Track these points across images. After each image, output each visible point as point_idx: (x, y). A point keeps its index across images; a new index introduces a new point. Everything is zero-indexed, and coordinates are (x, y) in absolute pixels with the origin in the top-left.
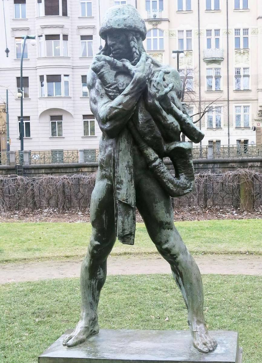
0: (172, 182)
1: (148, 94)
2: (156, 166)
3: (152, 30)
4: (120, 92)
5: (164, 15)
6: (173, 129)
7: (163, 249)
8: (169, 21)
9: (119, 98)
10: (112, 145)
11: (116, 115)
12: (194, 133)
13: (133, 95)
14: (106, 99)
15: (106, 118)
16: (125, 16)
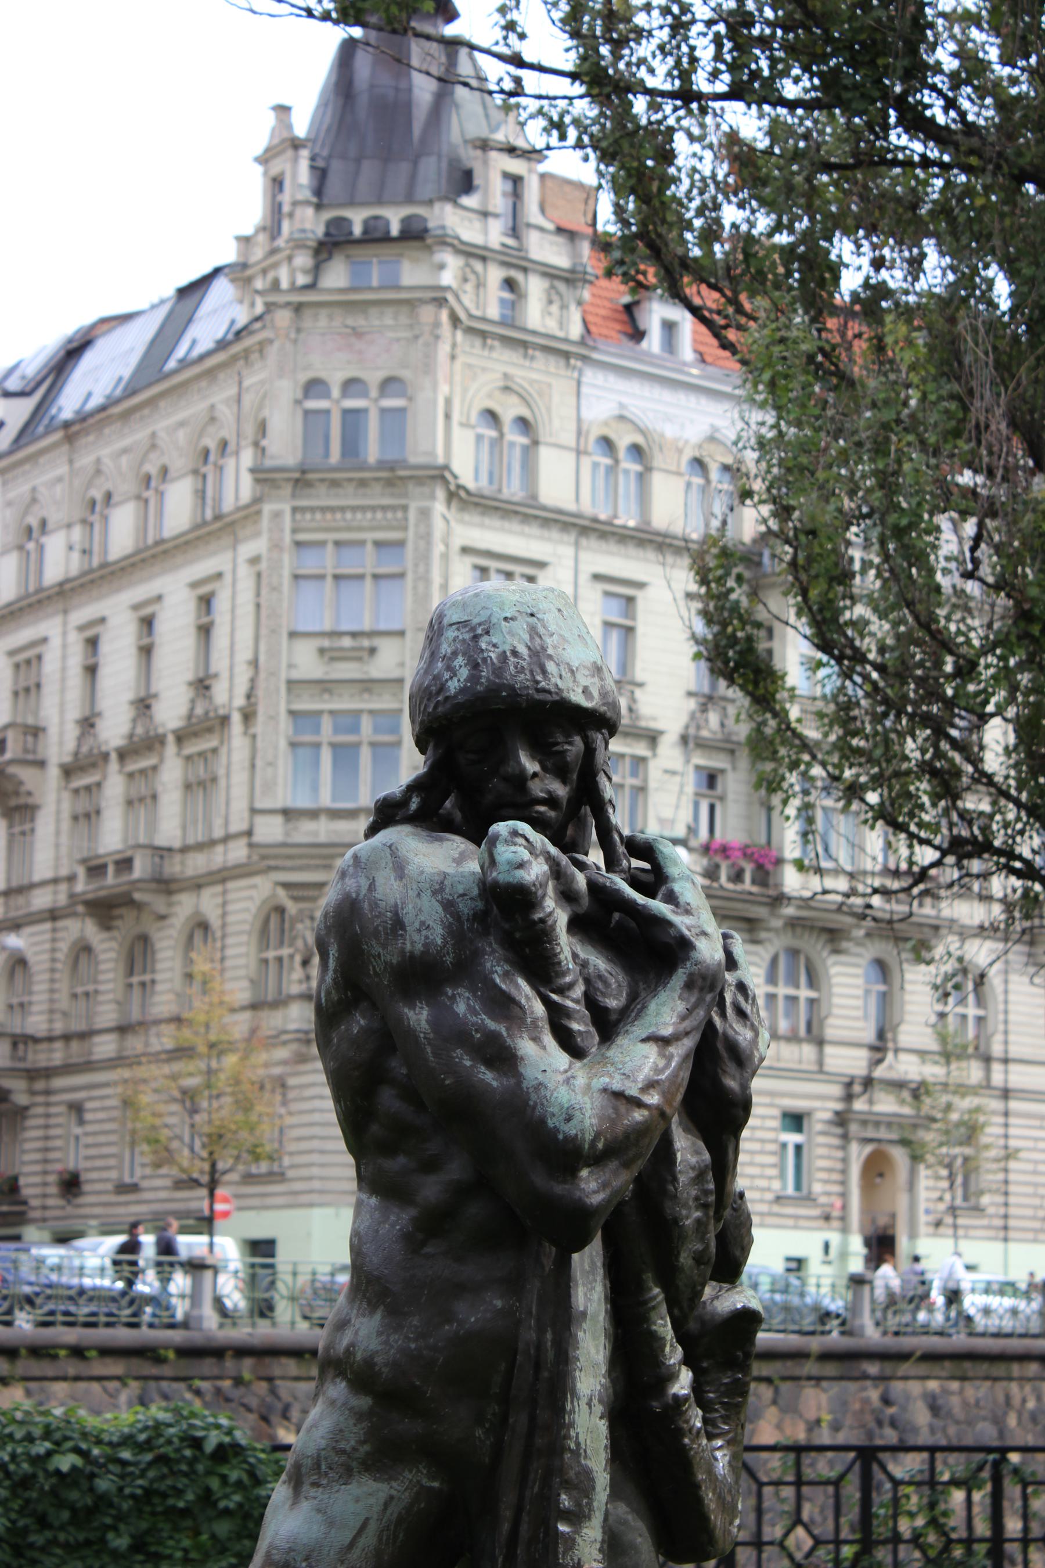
1: (720, 1046)
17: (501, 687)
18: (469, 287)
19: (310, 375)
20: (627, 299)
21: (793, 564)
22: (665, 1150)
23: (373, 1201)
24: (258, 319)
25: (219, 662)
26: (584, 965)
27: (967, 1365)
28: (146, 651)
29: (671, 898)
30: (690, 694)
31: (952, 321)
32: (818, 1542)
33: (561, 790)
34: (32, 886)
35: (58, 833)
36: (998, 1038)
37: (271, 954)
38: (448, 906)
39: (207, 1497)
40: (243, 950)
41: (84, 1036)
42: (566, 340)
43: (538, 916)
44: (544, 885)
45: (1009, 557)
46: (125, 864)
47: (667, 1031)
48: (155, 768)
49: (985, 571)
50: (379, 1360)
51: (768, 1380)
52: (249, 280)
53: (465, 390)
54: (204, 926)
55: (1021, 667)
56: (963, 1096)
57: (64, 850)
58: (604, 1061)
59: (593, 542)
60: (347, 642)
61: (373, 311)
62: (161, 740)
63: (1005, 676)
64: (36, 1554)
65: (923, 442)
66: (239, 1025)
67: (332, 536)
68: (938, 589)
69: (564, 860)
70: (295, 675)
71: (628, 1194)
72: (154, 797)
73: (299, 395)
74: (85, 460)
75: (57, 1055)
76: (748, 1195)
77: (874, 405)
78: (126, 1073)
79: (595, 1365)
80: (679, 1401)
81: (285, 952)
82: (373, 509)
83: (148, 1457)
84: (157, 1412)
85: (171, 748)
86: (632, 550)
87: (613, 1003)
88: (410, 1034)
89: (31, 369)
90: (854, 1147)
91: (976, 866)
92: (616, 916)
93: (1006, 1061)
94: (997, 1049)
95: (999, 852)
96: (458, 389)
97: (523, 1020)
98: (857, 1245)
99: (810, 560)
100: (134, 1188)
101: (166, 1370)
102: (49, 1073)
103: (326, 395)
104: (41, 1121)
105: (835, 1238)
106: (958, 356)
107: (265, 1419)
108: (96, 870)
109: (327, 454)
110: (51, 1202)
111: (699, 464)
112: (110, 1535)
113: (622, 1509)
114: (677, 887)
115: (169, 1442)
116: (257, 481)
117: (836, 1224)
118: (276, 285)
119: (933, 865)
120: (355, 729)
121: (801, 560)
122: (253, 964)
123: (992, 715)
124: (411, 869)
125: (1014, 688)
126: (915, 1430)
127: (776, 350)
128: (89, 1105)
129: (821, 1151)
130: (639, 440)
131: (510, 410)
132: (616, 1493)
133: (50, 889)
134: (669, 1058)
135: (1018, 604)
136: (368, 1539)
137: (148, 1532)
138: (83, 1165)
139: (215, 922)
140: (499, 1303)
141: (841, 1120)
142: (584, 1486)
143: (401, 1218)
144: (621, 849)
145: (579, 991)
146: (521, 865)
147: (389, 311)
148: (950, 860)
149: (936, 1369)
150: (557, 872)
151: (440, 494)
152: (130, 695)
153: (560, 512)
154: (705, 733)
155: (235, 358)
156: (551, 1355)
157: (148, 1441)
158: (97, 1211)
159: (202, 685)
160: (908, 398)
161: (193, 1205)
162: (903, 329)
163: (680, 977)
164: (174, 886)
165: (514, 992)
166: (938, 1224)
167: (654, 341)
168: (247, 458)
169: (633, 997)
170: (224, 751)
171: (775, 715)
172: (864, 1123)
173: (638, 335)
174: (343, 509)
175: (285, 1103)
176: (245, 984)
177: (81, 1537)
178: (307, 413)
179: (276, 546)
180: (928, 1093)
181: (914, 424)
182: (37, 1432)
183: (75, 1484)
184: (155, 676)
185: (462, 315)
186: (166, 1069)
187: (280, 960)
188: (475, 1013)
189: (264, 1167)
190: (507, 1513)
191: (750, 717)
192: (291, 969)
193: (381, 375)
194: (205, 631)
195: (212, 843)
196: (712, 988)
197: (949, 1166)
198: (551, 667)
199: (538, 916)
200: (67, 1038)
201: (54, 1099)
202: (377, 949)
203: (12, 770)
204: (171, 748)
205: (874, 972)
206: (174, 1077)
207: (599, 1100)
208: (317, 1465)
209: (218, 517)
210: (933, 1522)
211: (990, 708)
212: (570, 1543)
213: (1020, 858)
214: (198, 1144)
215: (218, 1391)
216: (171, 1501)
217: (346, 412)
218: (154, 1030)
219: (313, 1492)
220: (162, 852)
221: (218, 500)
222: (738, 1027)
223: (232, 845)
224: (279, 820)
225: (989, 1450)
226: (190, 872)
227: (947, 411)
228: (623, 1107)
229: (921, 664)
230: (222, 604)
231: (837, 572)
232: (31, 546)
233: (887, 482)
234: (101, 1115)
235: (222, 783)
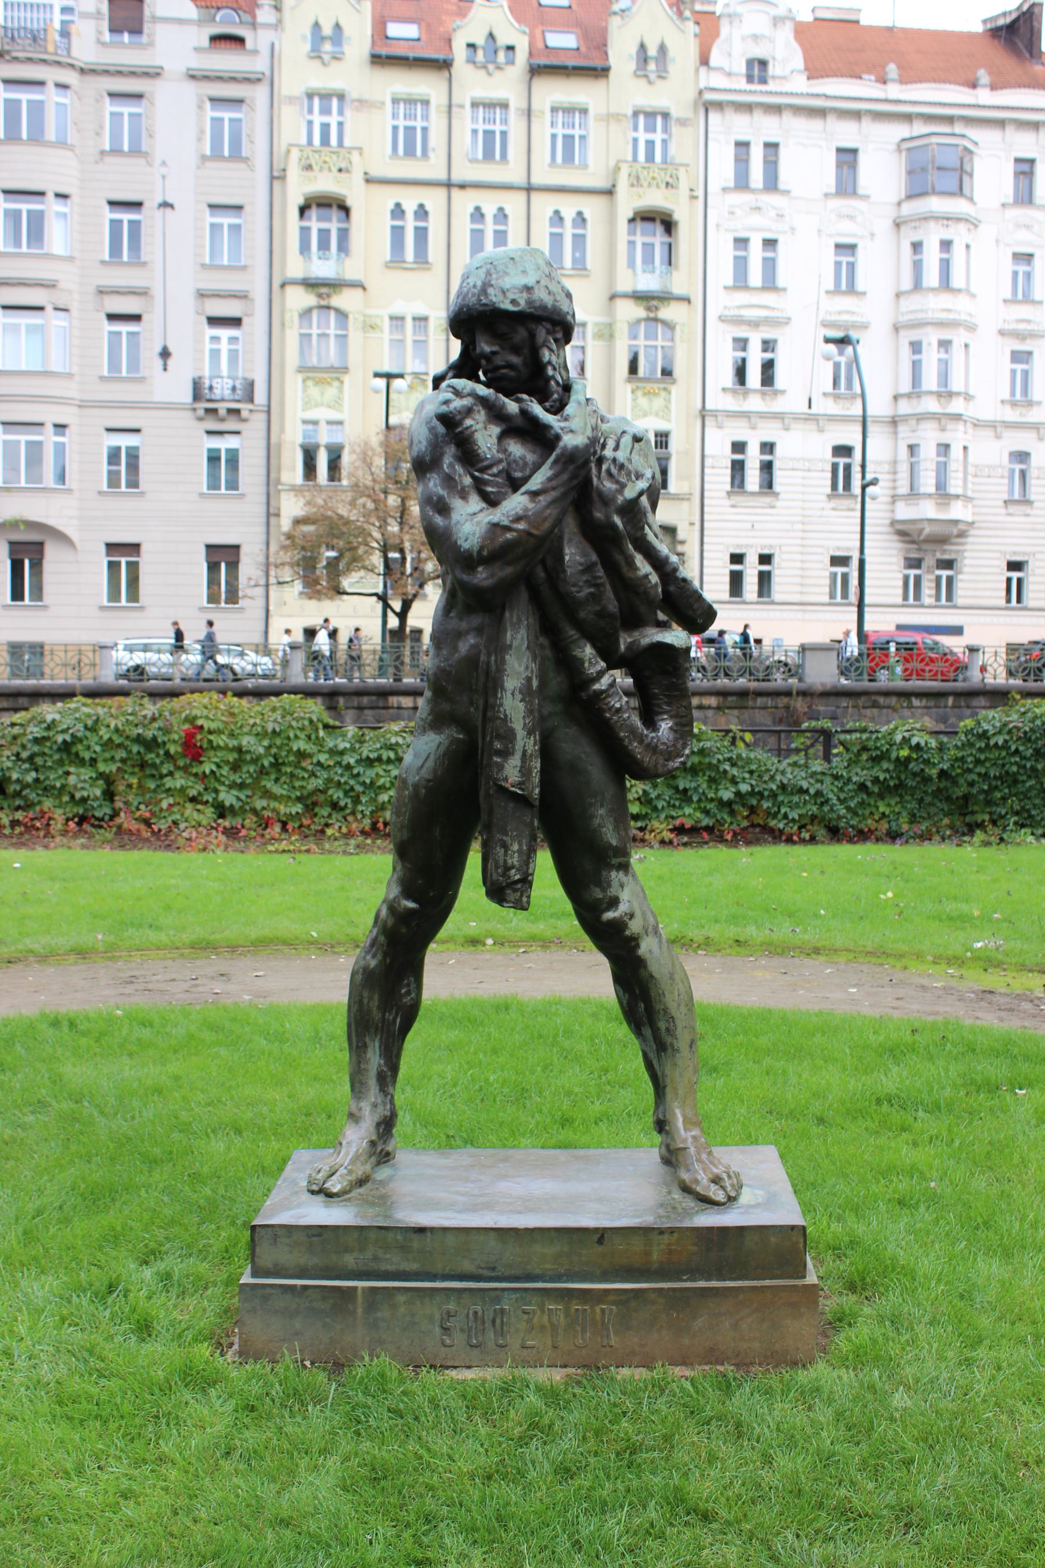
0: (641, 739)
1: (595, 495)
2: (602, 692)
3: (643, 325)
4: (515, 485)
5: (352, 270)
6: (646, 593)
7: (602, 923)
8: (364, 289)
9: (516, 503)
10: (479, 631)
11: (509, 546)
12: (696, 606)
13: (554, 494)
14: (475, 504)
15: (479, 552)
16: (530, 281)
136: (430, 763)
142: (509, 736)
212: (501, 767)
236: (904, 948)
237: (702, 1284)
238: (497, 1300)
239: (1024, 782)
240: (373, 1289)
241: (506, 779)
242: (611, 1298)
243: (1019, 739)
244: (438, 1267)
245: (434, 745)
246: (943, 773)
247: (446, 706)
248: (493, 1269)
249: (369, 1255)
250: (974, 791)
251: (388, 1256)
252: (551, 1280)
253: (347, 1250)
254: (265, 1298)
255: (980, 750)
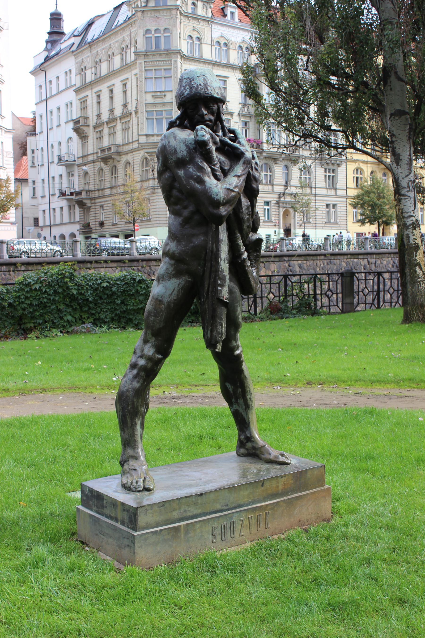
1: (252, 177)
17: (198, 93)
18: (184, 5)
19: (147, 28)
20: (223, 6)
21: (264, 68)
22: (240, 200)
23: (173, 216)
24: (133, 15)
25: (129, 100)
26: (219, 159)
27: (308, 257)
28: (111, 98)
29: (239, 143)
30: (240, 103)
31: (301, 7)
32: (275, 296)
33: (212, 118)
34: (88, 155)
35: (93, 142)
36: (314, 182)
37: (145, 169)
38: (187, 146)
39: (137, 291)
40: (138, 168)
41: (103, 190)
42: (208, 18)
43: (208, 148)
44: (209, 140)
45: (315, 65)
46: (109, 149)
47: (239, 174)
48: (115, 126)
49: (310, 69)
50: (176, 252)
51: (263, 262)
52: (131, 5)
53: (184, 31)
54: (129, 163)
55: (318, 92)
56: (306, 196)
57: (95, 146)
58: (225, 181)
59: (216, 67)
60: (159, 94)
61: (161, 12)
62: (116, 119)
63: (315, 94)
64: (100, 305)
65: (294, 38)
66: (138, 186)
67: (154, 68)
68: (299, 73)
69: (214, 134)
70: (147, 102)
71: (231, 212)
72: (115, 133)
73: (144, 33)
74: (94, 52)
75: (97, 194)
76: (259, 212)
77: (282, 28)
78: (113, 198)
79: (225, 252)
80: (244, 259)
81: (148, 168)
82: (163, 61)
83: (124, 283)
84: (125, 273)
85: (119, 121)
86: (225, 69)
87: (226, 168)
88: (179, 177)
89: (80, 29)
90: (281, 209)
91: (308, 140)
92: (226, 147)
93: (315, 188)
94: (313, 185)
95: (314, 137)
96: (182, 31)
97: (206, 172)
98: (282, 231)
99: (268, 67)
100: (116, 224)
101: (126, 265)
102: (95, 198)
103: (151, 33)
104: (94, 210)
105: (277, 230)
106: (302, 16)
107: (149, 275)
108: (103, 151)
109: (152, 48)
110: (97, 228)
111: (240, 47)
112: (116, 300)
113: (232, 284)
114: (240, 140)
115: (128, 279)
116: (135, 55)
117: (277, 227)
118: (137, 5)
119: (298, 140)
120: (162, 114)
121: (266, 67)
122: (141, 171)
123: (312, 104)
124: (178, 138)
125: (317, 97)
126: (296, 272)
127: (259, 15)
128: (105, 206)
129: (273, 210)
130: (226, 42)
131: (195, 35)
132: (231, 280)
133: (92, 155)
134: (240, 180)
135: (317, 77)
136: (175, 292)
137: (125, 299)
138: (104, 220)
139: (131, 162)
140: (203, 238)
141: (278, 203)
142: (224, 278)
143: (179, 220)
144: (227, 132)
145: (218, 165)
146: (204, 136)
147: (165, 12)
148: (303, 139)
149: (301, 258)
150: (212, 137)
151: (179, 57)
152: (108, 109)
153: (208, 60)
154: (244, 113)
155: (128, 25)
156: (215, 250)
157: (123, 279)
158: (108, 230)
159: (125, 105)
160: (290, 27)
161: (130, 228)
162: (289, 9)
163: (242, 161)
164: (121, 154)
165: (203, 166)
166: (300, 226)
167: (229, 17)
168: (133, 49)
169: (231, 166)
170: (131, 121)
171: (261, 106)
172: (283, 203)
173: (225, 16)
174: (156, 61)
175: (150, 204)
176: (139, 176)
177: (110, 301)
178: (146, 38)
179: (141, 71)
180: (298, 196)
181: (292, 33)
182: (98, 278)
183: (107, 289)
184: (114, 104)
185: (183, 12)
186: (122, 197)
187: (147, 170)
188: (194, 171)
189: (146, 218)
190: (206, 286)
191: (255, 106)
192: (150, 172)
193: (164, 28)
194: (125, 92)
195: (129, 143)
196: (249, 164)
197: (303, 213)
198: (209, 88)
199: (208, 148)
200: (98, 190)
201: (96, 205)
202: (171, 157)
203: (82, 128)
204: (119, 121)
205: (285, 168)
206: (124, 198)
207: (224, 191)
208: (163, 277)
209: (126, 65)
210: (301, 291)
211: (311, 102)
212: (221, 291)
213: (319, 138)
214: (130, 213)
215: (138, 269)
216: (129, 293)
217: (155, 37)
218: (118, 188)
219: (162, 282)
220: (118, 146)
221: (126, 60)
222: (256, 173)
223: (134, 143)
224: (145, 137)
225: (313, 275)
226: (125, 150)
227: (300, 30)
228: (229, 192)
229: (295, 92)
230: (128, 86)
231: (275, 70)
232: (83, 73)
233: (286, 47)
234: (108, 208)
235: (131, 129)
236: (85, 384)
237: (295, 495)
238: (232, 518)
239: (50, 306)
240: (187, 525)
241: (223, 297)
242: (269, 507)
243: (46, 285)
244: (208, 510)
245: (177, 284)
246: (10, 305)
247: (183, 267)
248: (227, 505)
249: (182, 510)
250: (26, 312)
251: (190, 509)
252: (247, 506)
253: (174, 510)
254: (146, 539)
255: (27, 292)
